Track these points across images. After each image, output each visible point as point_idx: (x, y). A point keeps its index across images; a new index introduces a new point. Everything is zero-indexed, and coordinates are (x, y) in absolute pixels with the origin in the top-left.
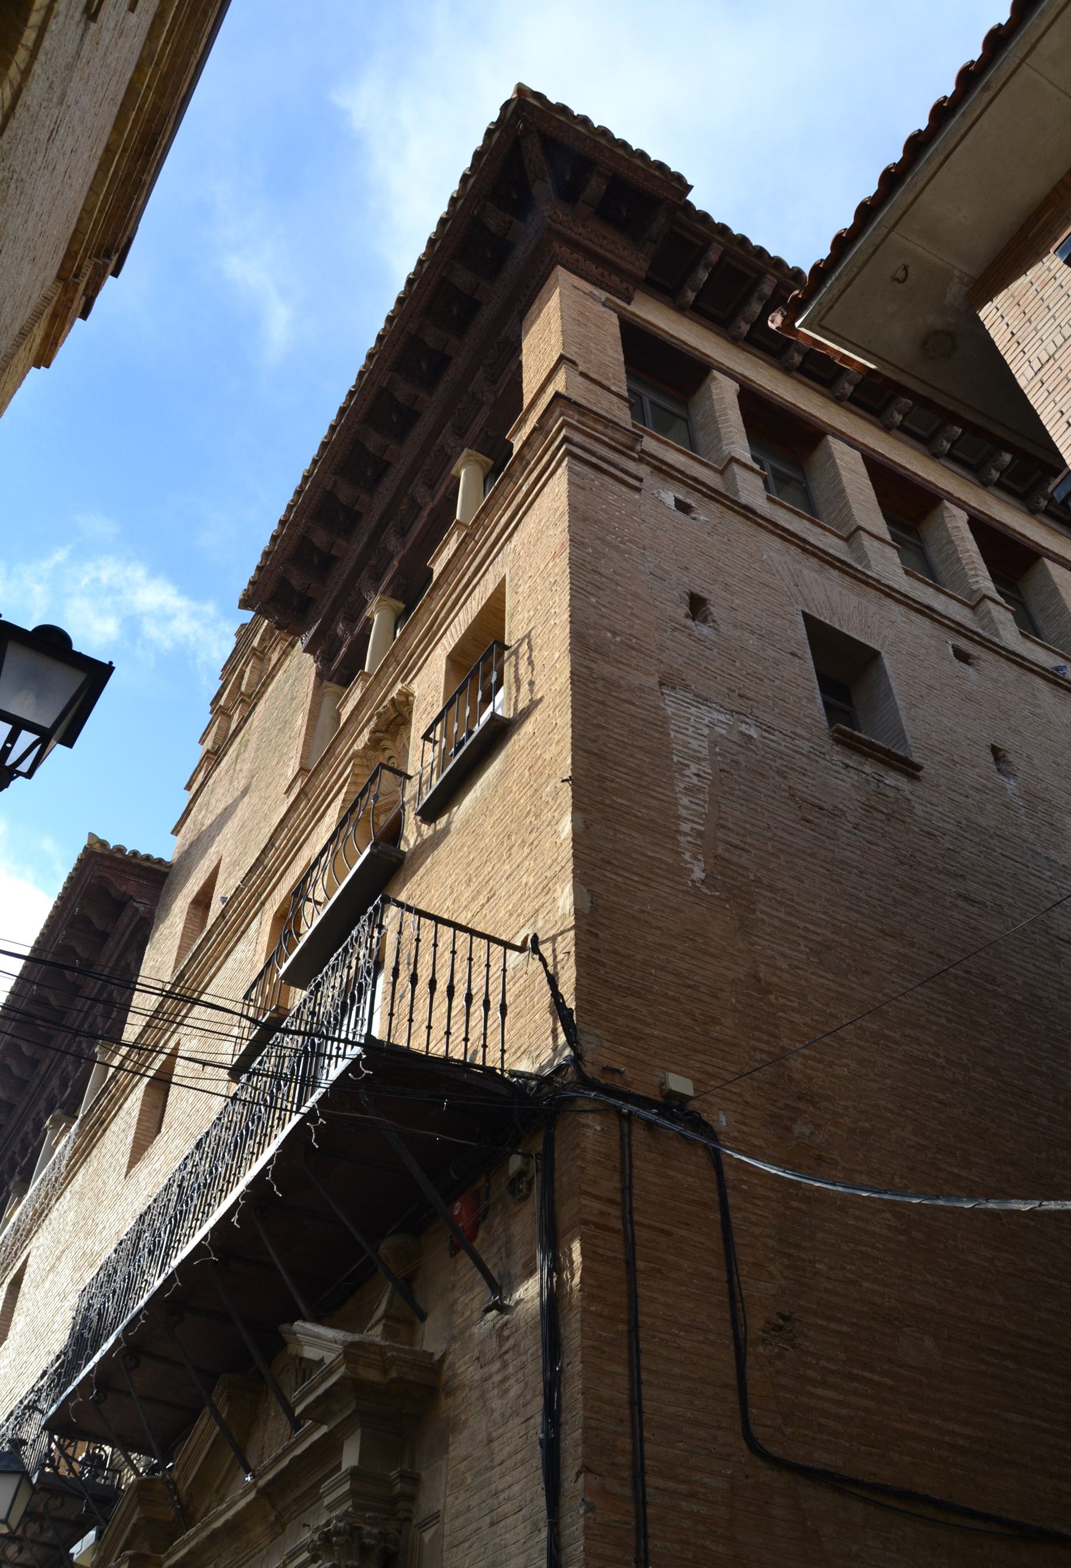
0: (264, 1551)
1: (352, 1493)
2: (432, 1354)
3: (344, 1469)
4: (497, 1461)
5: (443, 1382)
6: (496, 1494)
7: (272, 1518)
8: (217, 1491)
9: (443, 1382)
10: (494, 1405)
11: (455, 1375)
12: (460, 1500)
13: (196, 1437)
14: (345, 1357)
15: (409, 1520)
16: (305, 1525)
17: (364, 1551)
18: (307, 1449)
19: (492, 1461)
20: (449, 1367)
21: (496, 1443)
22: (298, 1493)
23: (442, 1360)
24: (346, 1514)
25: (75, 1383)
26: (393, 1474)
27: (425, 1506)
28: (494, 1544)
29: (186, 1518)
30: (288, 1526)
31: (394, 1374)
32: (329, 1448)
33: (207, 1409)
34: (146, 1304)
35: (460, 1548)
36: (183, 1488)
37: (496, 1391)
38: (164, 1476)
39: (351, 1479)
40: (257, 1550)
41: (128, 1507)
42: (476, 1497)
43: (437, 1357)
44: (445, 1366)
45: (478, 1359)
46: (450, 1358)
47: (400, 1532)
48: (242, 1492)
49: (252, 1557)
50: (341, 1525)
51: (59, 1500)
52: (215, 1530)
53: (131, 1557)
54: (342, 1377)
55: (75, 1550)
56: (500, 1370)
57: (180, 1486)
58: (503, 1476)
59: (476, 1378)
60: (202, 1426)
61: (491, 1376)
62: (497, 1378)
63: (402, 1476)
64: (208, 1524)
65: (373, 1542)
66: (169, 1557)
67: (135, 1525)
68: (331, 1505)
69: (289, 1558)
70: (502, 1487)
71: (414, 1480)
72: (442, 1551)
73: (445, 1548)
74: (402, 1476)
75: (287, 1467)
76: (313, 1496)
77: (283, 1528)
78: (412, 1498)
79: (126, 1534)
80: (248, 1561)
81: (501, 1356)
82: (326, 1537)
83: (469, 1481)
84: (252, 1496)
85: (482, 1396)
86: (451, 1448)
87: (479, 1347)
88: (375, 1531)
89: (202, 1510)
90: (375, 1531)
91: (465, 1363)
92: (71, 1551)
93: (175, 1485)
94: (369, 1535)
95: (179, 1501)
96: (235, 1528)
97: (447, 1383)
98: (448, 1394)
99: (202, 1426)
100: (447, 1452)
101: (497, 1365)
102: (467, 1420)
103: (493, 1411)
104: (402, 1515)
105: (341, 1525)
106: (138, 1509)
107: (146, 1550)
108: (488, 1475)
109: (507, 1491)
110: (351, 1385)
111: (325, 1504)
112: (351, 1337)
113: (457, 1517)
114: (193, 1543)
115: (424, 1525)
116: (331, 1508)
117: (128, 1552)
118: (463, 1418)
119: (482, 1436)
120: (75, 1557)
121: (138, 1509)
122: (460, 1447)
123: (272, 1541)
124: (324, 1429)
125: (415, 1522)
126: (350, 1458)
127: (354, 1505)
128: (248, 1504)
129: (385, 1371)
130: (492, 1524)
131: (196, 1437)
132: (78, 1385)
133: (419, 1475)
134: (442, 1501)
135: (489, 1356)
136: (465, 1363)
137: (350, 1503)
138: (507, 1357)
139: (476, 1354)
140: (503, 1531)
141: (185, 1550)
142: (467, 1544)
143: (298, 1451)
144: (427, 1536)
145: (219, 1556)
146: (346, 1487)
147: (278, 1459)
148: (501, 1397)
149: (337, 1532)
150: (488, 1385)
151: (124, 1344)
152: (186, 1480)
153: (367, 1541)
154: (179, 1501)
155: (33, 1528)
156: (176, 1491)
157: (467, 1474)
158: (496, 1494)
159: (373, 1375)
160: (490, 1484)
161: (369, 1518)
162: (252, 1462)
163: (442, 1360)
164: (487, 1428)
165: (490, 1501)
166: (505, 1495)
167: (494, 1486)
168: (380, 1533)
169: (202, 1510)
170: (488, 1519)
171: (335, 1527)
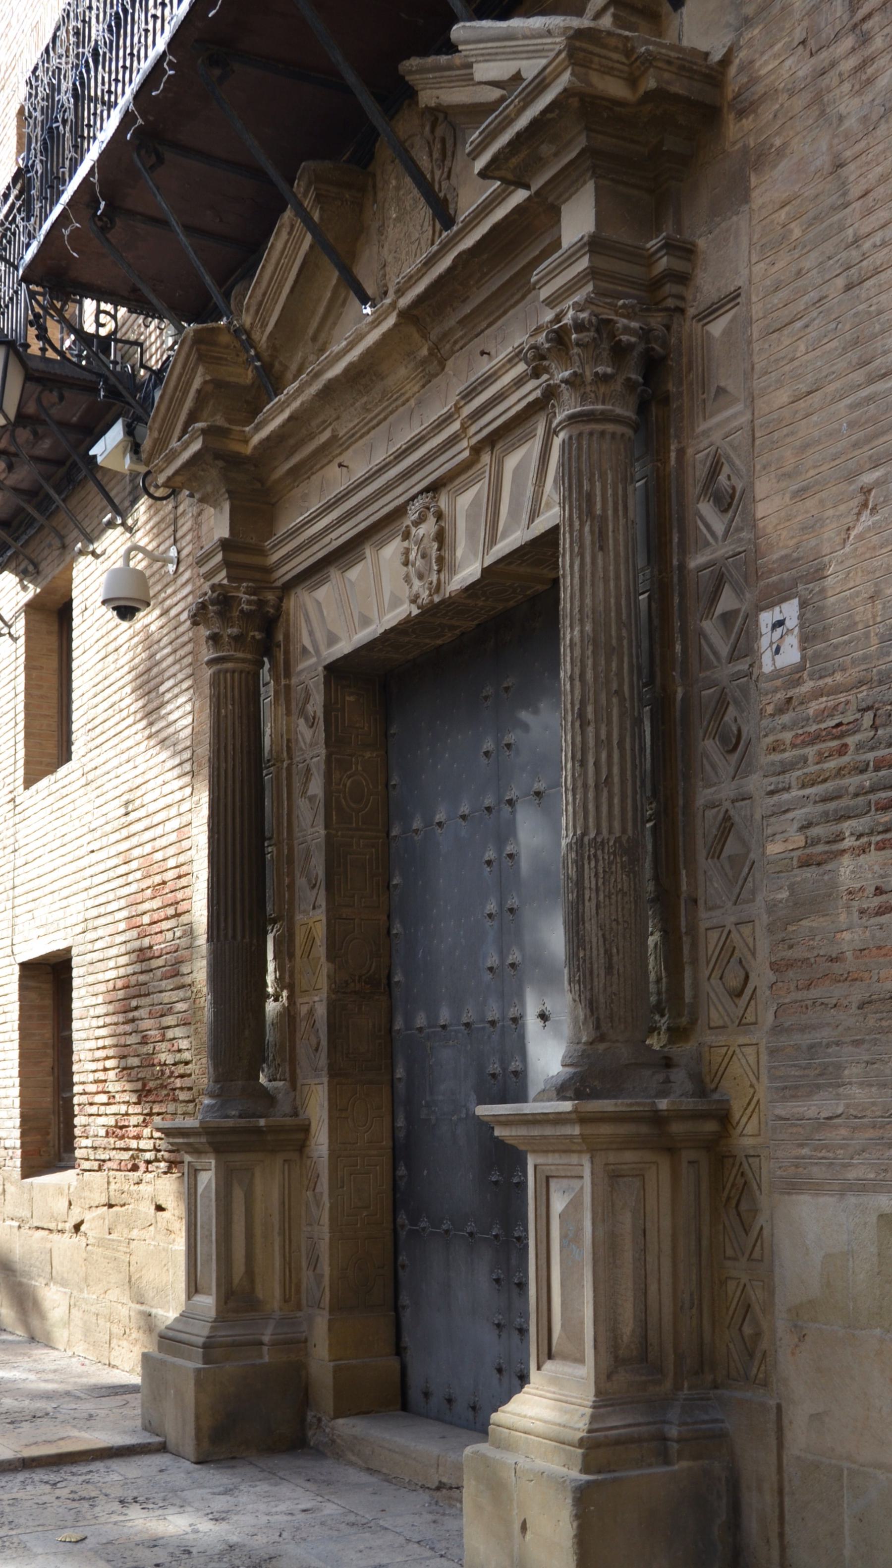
0: (412, 402)
1: (592, 273)
2: (707, 54)
3: (565, 245)
4: (855, 191)
5: (730, 95)
6: (857, 241)
7: (425, 352)
8: (314, 339)
9: (730, 95)
10: (842, 109)
11: (754, 80)
12: (780, 265)
13: (273, 261)
14: (570, 56)
15: (682, 311)
16: (483, 353)
17: (619, 352)
18: (484, 237)
19: (845, 194)
20: (741, 69)
21: (852, 166)
22: (467, 309)
23: (725, 61)
24: (589, 301)
25: (65, 198)
26: (653, 244)
27: (708, 284)
28: (856, 315)
29: (270, 381)
30: (450, 363)
31: (650, 83)
32: (540, 217)
33: (288, 215)
34: (171, 44)
35: (786, 332)
36: (262, 338)
37: (846, 87)
38: (230, 323)
39: (590, 251)
40: (399, 402)
41: (184, 368)
42: (813, 255)
43: (716, 57)
44: (733, 70)
45: (803, 42)
46: (742, 55)
47: (668, 328)
48: (364, 327)
49: (392, 413)
50: (584, 315)
51: (55, 393)
52: (330, 380)
53: (204, 432)
54: (565, 90)
55: (98, 450)
56: (854, 49)
57: (256, 336)
58: (870, 212)
59: (801, 74)
60: (279, 246)
61: (833, 64)
62: (847, 65)
63: (669, 246)
64: (317, 375)
65: (633, 339)
66: (257, 429)
67: (199, 391)
68: (559, 292)
69: (463, 398)
70: (868, 230)
71: (686, 251)
72: (750, 342)
73: (755, 335)
74: (669, 246)
75: (450, 270)
76: (519, 287)
77: (442, 366)
78: (684, 279)
79: (189, 403)
80: (385, 419)
81: (855, 26)
82: (559, 338)
83: (797, 232)
84: (391, 321)
85: (818, 99)
86: (754, 194)
87: (805, 23)
88: (634, 325)
89: (294, 367)
90: (634, 325)
91: (776, 56)
92: (92, 453)
93: (248, 334)
94: (627, 330)
95: (258, 357)
96: (362, 375)
97: (739, 94)
98: (741, 114)
99: (279, 246)
100: (746, 198)
101: (848, 42)
102: (785, 145)
103: (841, 118)
104: (670, 303)
105: (584, 315)
106: (201, 370)
107: (220, 421)
108: (835, 218)
109: (880, 234)
110: (581, 106)
111: (542, 298)
112: (575, 22)
113: (777, 289)
114: (296, 405)
115: (711, 312)
116: (551, 302)
117: (199, 425)
118: (778, 142)
119: (823, 161)
120: (99, 460)
121: (201, 370)
122: (769, 189)
123: (423, 386)
124: (520, 196)
125: (691, 312)
126: (578, 221)
127: (228, 576)
128: (384, 335)
129: (633, 82)
130: (849, 287)
131: (273, 261)
132: (69, 204)
133: (694, 245)
134: (745, 272)
135: (828, 32)
136: (776, 56)
137: (590, 287)
138: (866, 26)
139: (799, 34)
140: (873, 292)
141: (286, 415)
142: (799, 325)
143: (469, 242)
144: (717, 328)
145: (338, 418)
146: (584, 263)
147: (411, 280)
148: (859, 92)
149: (579, 326)
150: (832, 78)
151: (140, 121)
152: (264, 325)
153: (625, 338)
154: (258, 357)
155: (24, 435)
156: (250, 343)
157: (792, 225)
158: (857, 241)
159: (614, 88)
160: (842, 229)
161: (624, 306)
162: (370, 290)
163: (725, 61)
164: (831, 147)
165: (844, 255)
166: (877, 238)
167: (850, 231)
168: (641, 328)
169: (294, 367)
170: (840, 282)
171: (575, 320)
